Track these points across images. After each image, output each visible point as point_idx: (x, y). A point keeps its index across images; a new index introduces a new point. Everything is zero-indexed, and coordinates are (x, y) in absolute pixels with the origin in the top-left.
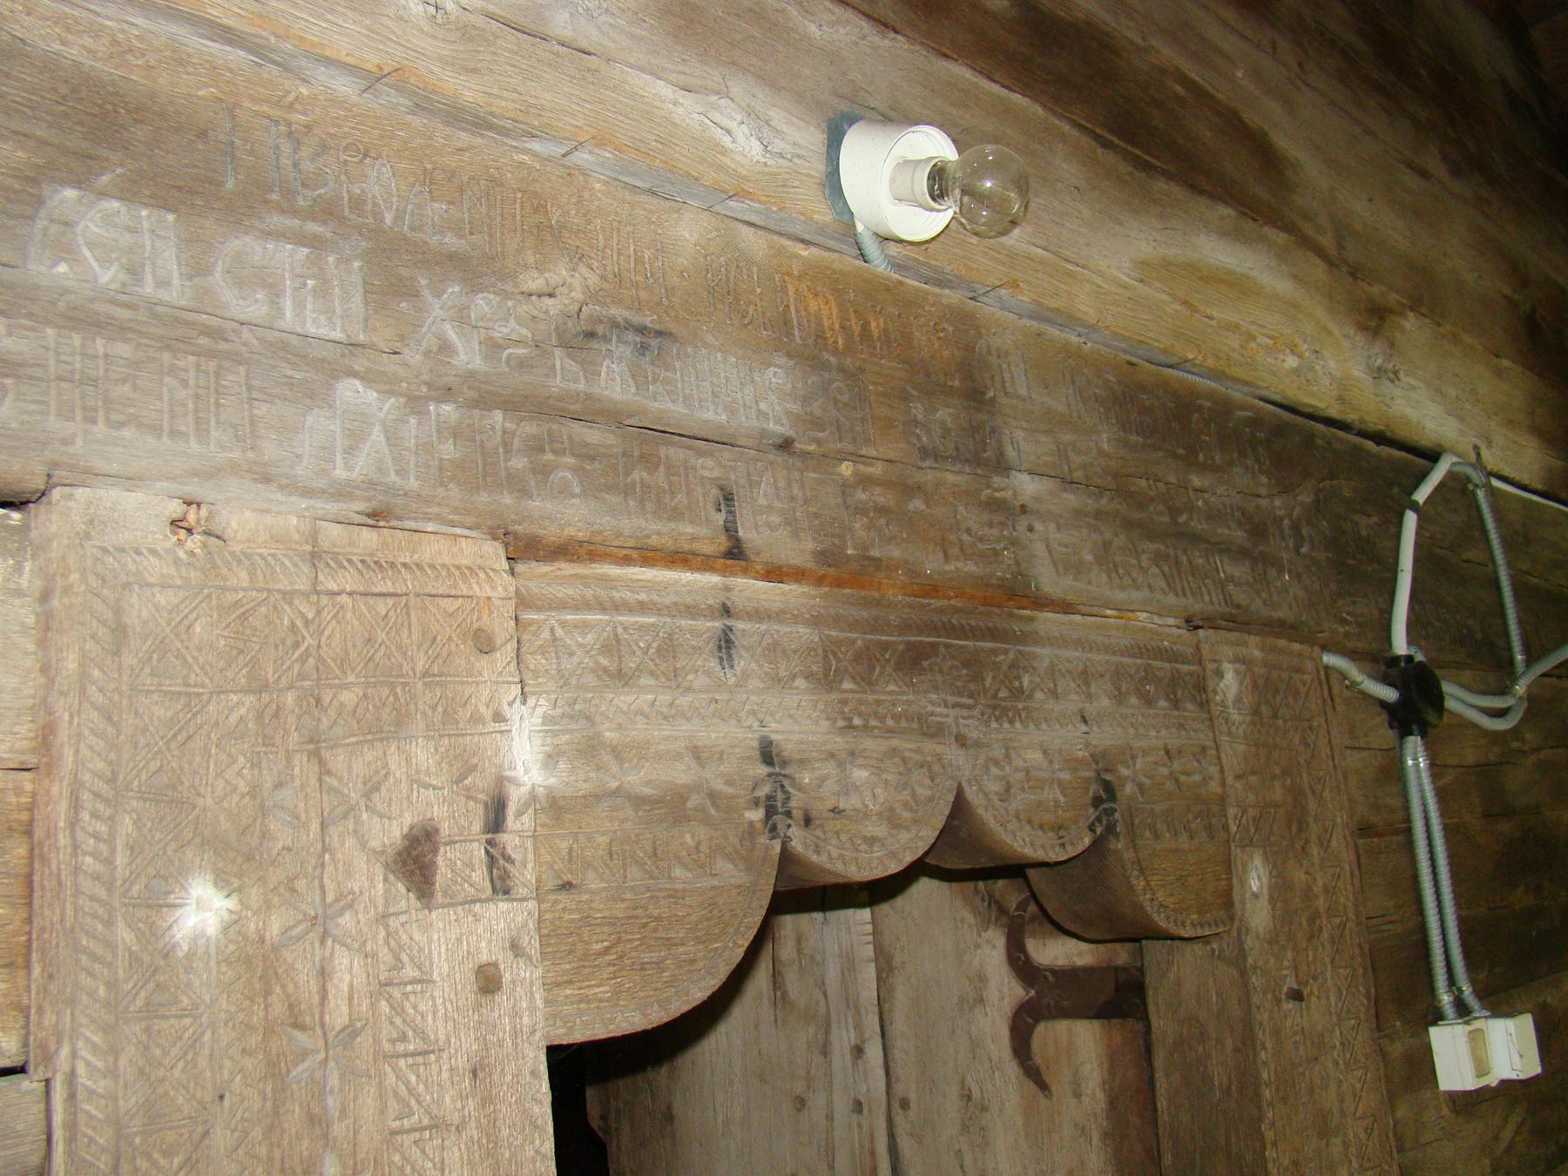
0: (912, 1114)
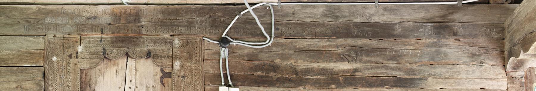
0: (138, 88)
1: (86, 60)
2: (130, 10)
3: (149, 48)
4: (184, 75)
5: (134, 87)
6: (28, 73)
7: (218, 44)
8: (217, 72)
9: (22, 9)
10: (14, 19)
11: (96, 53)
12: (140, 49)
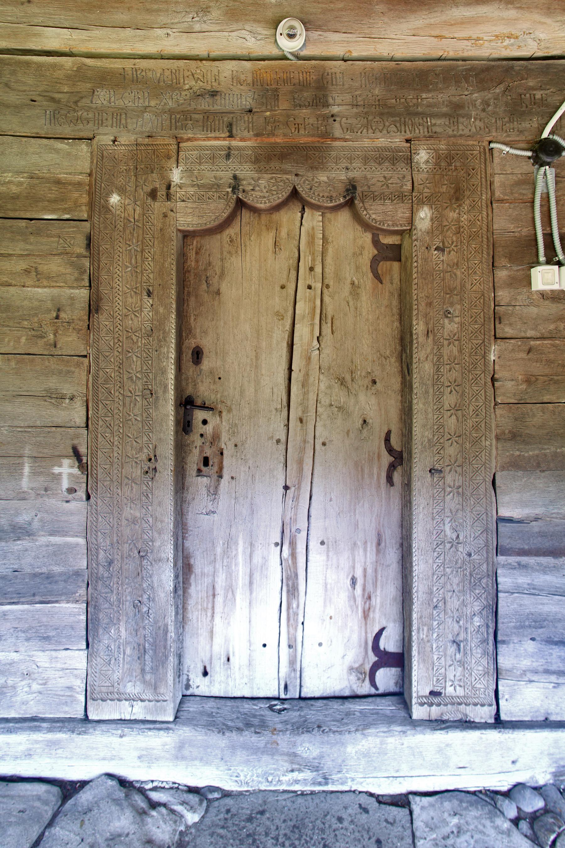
0: (330, 289)
1: (190, 205)
2: (301, 75)
3: (351, 174)
4: (441, 245)
5: (320, 285)
6: (52, 237)
7: (529, 158)
8: (525, 231)
9: (40, 66)
10: (21, 93)
11: (216, 187)
12: (328, 178)
